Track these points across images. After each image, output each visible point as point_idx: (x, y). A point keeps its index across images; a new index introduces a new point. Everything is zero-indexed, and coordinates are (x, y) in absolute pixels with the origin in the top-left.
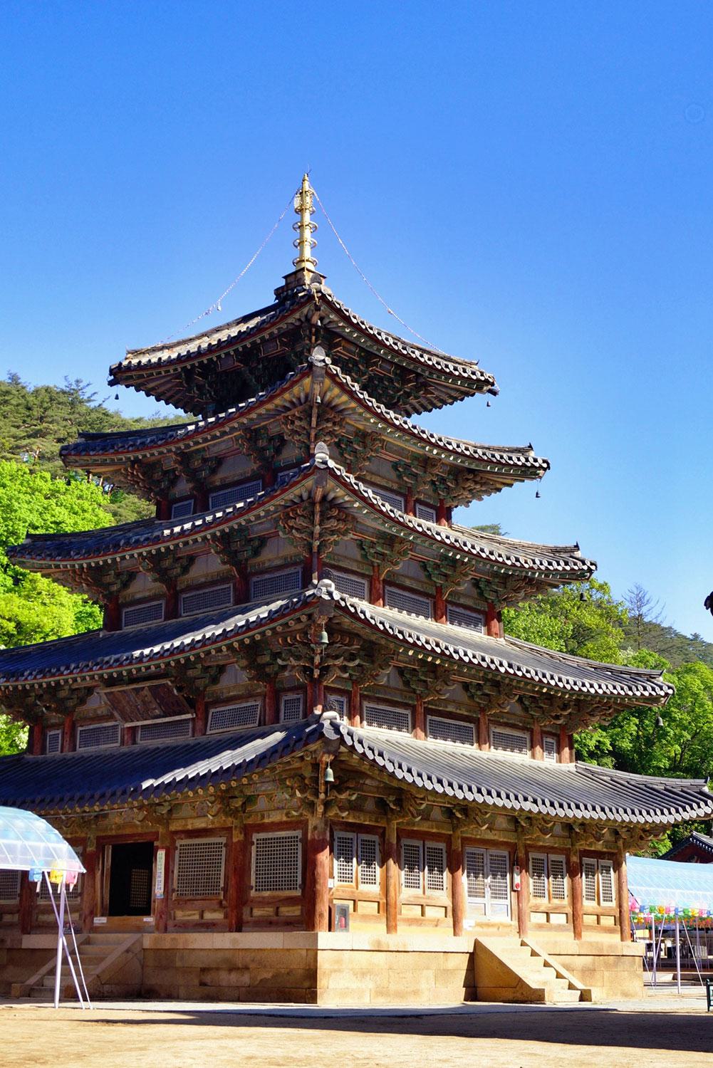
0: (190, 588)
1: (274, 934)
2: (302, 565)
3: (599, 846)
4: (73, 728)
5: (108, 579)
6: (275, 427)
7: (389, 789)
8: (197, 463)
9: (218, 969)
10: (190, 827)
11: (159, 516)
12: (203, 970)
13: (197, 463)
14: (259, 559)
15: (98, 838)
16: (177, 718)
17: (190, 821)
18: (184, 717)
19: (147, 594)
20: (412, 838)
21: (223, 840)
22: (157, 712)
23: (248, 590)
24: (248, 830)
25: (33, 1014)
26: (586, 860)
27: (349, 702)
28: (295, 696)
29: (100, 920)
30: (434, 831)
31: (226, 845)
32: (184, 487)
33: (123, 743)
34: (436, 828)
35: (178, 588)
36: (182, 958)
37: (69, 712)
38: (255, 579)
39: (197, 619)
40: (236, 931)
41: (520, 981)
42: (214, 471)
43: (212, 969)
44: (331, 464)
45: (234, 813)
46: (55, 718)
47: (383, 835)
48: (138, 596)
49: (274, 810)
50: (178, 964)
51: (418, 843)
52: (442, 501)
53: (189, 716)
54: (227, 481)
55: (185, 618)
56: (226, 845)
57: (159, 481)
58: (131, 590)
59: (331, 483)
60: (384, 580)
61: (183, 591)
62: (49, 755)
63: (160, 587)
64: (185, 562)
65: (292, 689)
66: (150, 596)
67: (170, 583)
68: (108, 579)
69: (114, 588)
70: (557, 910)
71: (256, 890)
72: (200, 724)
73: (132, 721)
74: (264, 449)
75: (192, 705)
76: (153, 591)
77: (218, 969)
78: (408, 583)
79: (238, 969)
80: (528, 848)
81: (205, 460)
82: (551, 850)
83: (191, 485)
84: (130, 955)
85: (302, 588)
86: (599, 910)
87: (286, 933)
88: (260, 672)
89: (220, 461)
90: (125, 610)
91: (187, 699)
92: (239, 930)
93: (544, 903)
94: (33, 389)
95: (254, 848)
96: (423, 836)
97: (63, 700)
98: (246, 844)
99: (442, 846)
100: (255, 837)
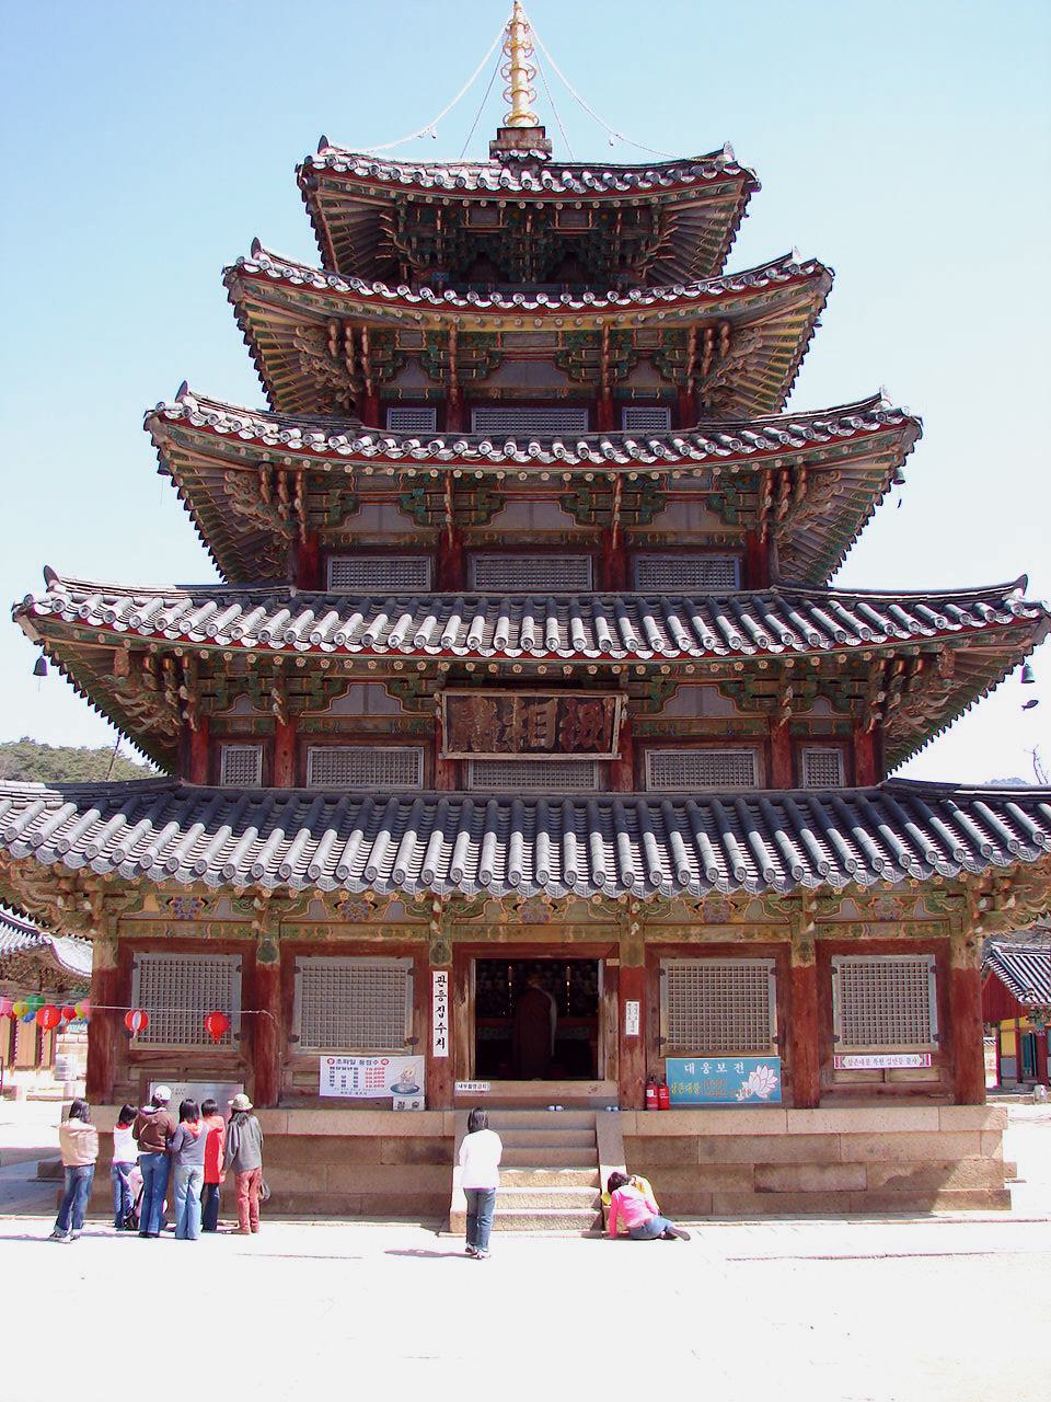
1: (920, 1109)
2: (741, 554)
6: (648, 338)
10: (693, 940)
12: (762, 1167)
15: (457, 947)
17: (694, 930)
19: (392, 541)
29: (467, 1087)
30: (380, 939)
31: (774, 971)
34: (383, 935)
35: (467, 543)
36: (711, 1152)
40: (956, 1104)
49: (875, 921)
50: (703, 1159)
56: (774, 971)
58: (351, 526)
66: (397, 546)
71: (139, 1040)
72: (627, 772)
73: (470, 750)
76: (407, 538)
79: (841, 1164)
87: (944, 1108)
98: (824, 971)
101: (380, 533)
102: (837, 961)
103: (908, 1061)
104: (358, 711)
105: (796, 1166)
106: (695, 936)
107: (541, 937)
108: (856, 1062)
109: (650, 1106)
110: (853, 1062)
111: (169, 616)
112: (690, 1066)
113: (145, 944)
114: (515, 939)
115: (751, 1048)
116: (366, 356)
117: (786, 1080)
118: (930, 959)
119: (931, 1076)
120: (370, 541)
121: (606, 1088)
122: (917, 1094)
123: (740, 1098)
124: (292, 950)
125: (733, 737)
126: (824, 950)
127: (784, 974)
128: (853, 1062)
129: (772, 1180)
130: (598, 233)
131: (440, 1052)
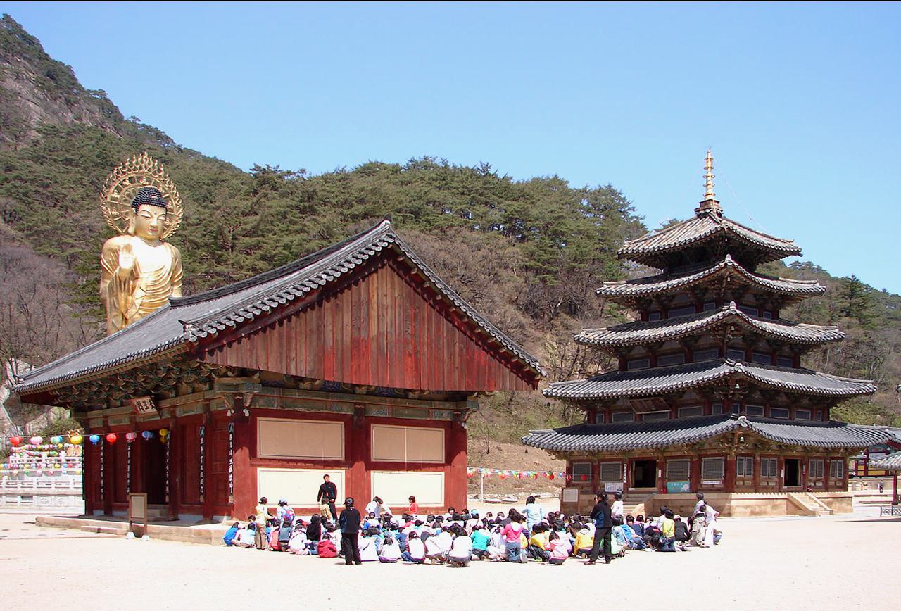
0: (663, 355)
3: (839, 455)
4: (610, 414)
7: (759, 440)
12: (681, 506)
22: (654, 409)
26: (832, 461)
28: (718, 404)
33: (636, 420)
36: (671, 503)
38: (696, 353)
39: (668, 369)
41: (225, 167)
43: (547, 450)
44: (738, 312)
47: (754, 457)
51: (767, 459)
58: (632, 353)
59: (738, 318)
61: (659, 356)
62: (598, 424)
65: (717, 402)
70: (819, 480)
72: (673, 414)
75: (670, 406)
77: (688, 506)
80: (666, 458)
82: (819, 458)
86: (836, 480)
90: (629, 362)
93: (814, 478)
94: (857, 488)
95: (703, 463)
96: (769, 456)
98: (700, 461)
99: (776, 459)
101: (639, 354)
102: (703, 459)
103: (716, 482)
104: (621, 404)
105: (688, 506)
106: (674, 454)
107: (644, 456)
108: (706, 483)
109: (307, 519)
110: (705, 483)
111: (554, 391)
112: (672, 484)
113: (575, 461)
114: (641, 456)
115: (682, 479)
116: (167, 485)
117: (691, 487)
118: (723, 458)
119: (722, 486)
120: (636, 356)
121: (655, 489)
122: (718, 490)
123: (681, 491)
124: (600, 461)
125: (697, 403)
126: (700, 456)
127: (692, 462)
128: (705, 483)
129: (683, 509)
130: (737, 248)
131: (625, 482)
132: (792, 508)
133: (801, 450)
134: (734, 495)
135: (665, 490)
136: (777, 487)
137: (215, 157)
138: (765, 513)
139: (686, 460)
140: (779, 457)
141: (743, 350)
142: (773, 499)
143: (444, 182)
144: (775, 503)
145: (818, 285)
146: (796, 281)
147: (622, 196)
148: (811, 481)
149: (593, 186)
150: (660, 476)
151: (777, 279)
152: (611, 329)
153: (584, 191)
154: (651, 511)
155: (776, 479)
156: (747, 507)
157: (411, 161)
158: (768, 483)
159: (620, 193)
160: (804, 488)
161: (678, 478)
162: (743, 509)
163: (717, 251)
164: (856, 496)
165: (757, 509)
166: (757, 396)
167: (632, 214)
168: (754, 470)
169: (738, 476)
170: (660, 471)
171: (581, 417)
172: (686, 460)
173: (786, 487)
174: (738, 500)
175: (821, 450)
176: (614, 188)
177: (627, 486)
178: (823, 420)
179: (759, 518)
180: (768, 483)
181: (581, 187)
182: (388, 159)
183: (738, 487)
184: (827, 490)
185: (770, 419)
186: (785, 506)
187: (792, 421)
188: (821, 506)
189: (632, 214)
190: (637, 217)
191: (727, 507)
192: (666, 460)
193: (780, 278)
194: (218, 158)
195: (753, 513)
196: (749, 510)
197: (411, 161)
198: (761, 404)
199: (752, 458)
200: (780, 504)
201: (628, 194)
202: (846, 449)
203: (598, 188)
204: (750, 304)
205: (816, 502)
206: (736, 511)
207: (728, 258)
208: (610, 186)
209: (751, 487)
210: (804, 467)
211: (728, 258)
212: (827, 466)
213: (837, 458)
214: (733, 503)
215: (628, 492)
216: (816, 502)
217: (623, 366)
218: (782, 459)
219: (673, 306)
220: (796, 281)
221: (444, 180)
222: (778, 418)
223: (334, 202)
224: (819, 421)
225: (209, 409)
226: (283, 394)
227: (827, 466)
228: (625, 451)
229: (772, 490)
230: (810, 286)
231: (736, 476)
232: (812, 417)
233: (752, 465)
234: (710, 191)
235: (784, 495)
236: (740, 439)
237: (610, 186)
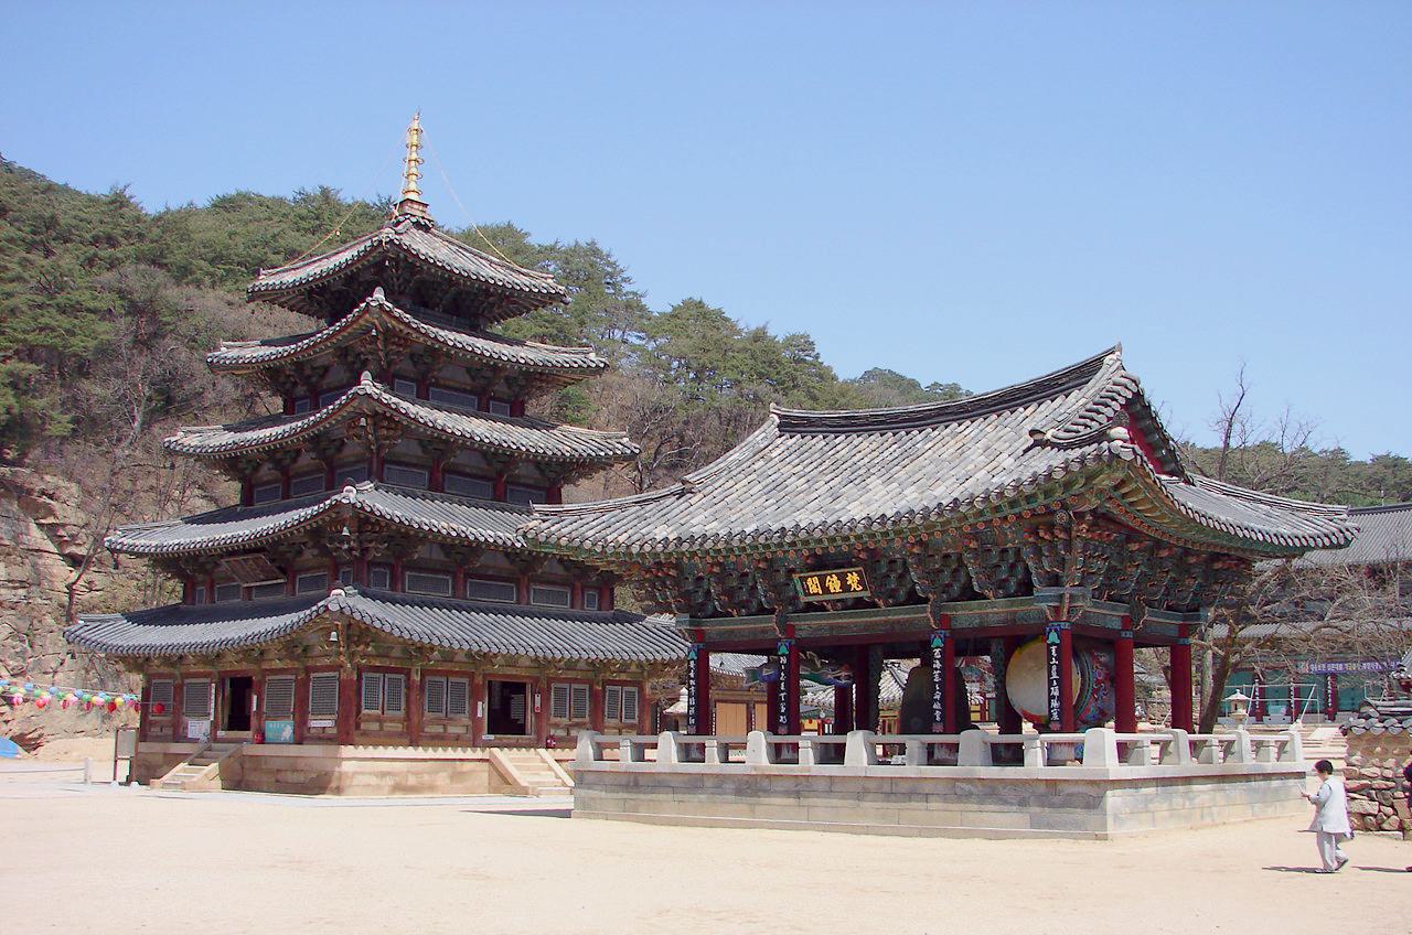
4: (212, 587)
5: (241, 465)
8: (308, 372)
9: (286, 770)
11: (285, 412)
13: (308, 372)
14: (296, 466)
16: (275, 582)
18: (279, 581)
20: (435, 675)
21: (293, 677)
22: (262, 577)
23: (252, 497)
24: (308, 670)
25: (324, 803)
27: (392, 573)
29: (221, 734)
32: (301, 390)
37: (208, 573)
38: (339, 471)
42: (323, 376)
45: (297, 658)
46: (200, 577)
48: (265, 479)
52: (517, 396)
53: (282, 581)
54: (332, 386)
55: (257, 506)
57: (285, 383)
60: (443, 469)
61: (294, 477)
63: (277, 474)
64: (293, 455)
67: (284, 471)
68: (241, 465)
69: (247, 472)
72: (290, 587)
74: (310, 376)
75: (283, 571)
77: (286, 770)
78: (468, 470)
80: (550, 680)
81: (313, 369)
82: (575, 680)
83: (305, 388)
84: (232, 759)
85: (327, 490)
88: (324, 551)
89: (326, 369)
91: (279, 568)
92: (300, 743)
93: (565, 721)
97: (203, 564)
99: (465, 680)
100: (312, 675)
128: (313, 724)
132: (496, 779)
133: (528, 663)
134: (347, 751)
135: (262, 739)
136: (470, 736)
137: (66, 185)
138: (432, 788)
139: (289, 677)
140: (471, 676)
141: (423, 467)
142: (454, 760)
143: (318, 222)
144: (459, 769)
145: (592, 356)
146: (556, 348)
147: (612, 260)
148: (557, 726)
149: (566, 241)
150: (255, 709)
151: (521, 343)
152: (228, 428)
153: (552, 249)
154: (237, 778)
155: (465, 719)
156: (383, 774)
157: (300, 193)
158: (445, 728)
159: (608, 256)
160: (539, 740)
161: (278, 714)
162: (373, 780)
163: (393, 285)
164: (1301, 775)
165: (412, 781)
166: (378, 551)
167: (627, 288)
168: (408, 701)
169: (364, 711)
170: (255, 697)
171: (172, 592)
172: (289, 677)
173: (492, 737)
174: (354, 760)
175: (461, 657)
176: (599, 246)
177: (215, 726)
178: (600, 609)
179: (413, 798)
180: (445, 728)
181: (548, 242)
182: (268, 190)
183: (365, 734)
184: (414, 743)
185: (470, 603)
186: (486, 775)
187: (399, 595)
188: (557, 777)
189: (627, 288)
190: (635, 294)
191: (336, 774)
192: (264, 676)
193: (528, 343)
194: (71, 186)
195: (399, 788)
196: (389, 781)
197: (300, 193)
198: (447, 572)
199: (402, 677)
200: (473, 771)
201: (620, 257)
202: (640, 665)
203: (572, 244)
204: (457, 385)
205: (550, 769)
206: (355, 782)
207: (379, 294)
208: (593, 243)
209: (401, 735)
210: (538, 699)
211: (379, 294)
212: (597, 699)
213: (623, 683)
214: (347, 767)
215: (216, 740)
216: (550, 769)
217: (248, 498)
218: (479, 680)
219: (325, 387)
220: (556, 348)
221: (317, 219)
222: (485, 601)
223: (88, 236)
224: (593, 611)
225: (1115, 659)
226: (393, 588)
227: (597, 699)
228: (212, 655)
229: (457, 741)
230: (579, 358)
231: (359, 712)
232: (572, 600)
233: (403, 690)
234: (413, 186)
235: (479, 754)
236: (329, 635)
237: (593, 243)
